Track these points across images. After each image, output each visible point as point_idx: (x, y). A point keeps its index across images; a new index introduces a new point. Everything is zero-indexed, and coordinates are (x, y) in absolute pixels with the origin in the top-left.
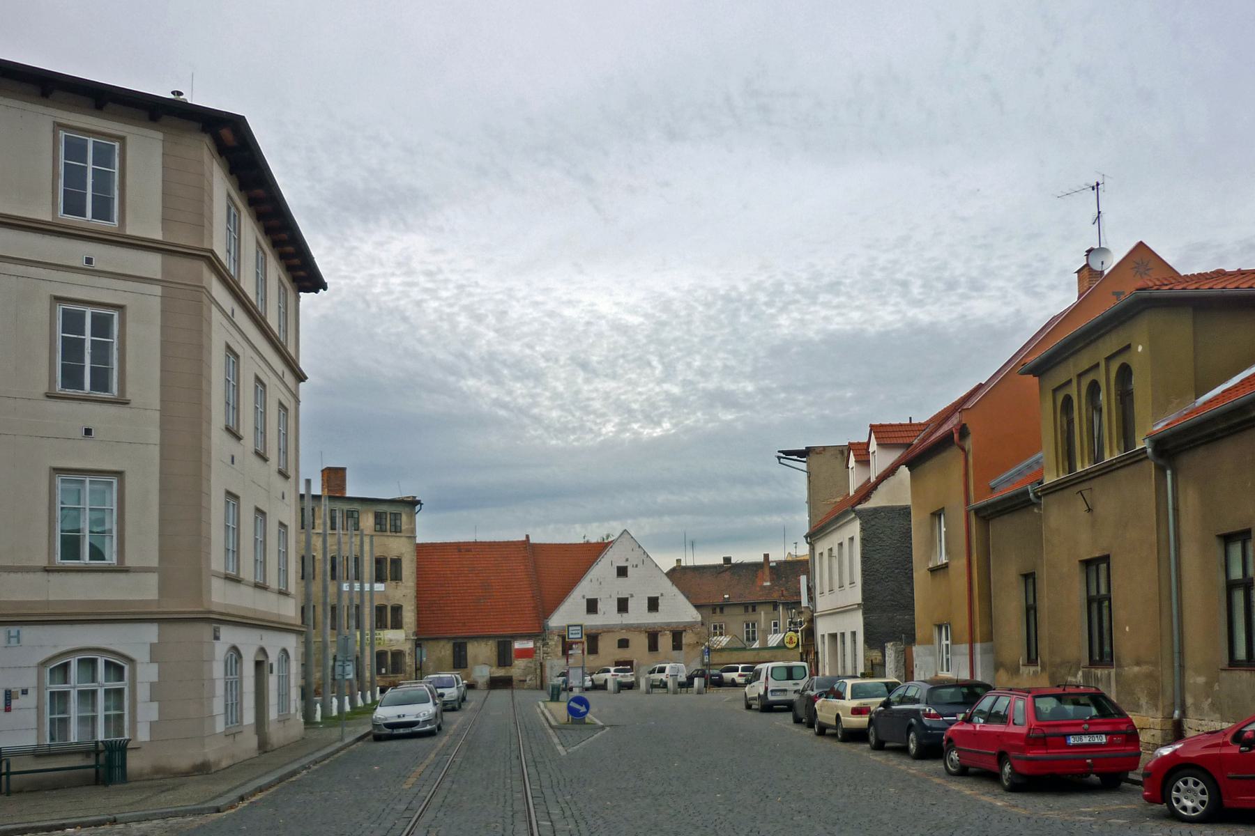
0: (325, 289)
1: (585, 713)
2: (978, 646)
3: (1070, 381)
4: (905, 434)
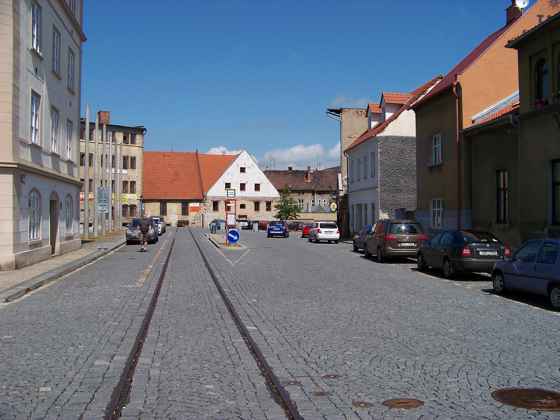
1: (236, 240)
2: (463, 212)
3: (546, 49)
4: (401, 99)
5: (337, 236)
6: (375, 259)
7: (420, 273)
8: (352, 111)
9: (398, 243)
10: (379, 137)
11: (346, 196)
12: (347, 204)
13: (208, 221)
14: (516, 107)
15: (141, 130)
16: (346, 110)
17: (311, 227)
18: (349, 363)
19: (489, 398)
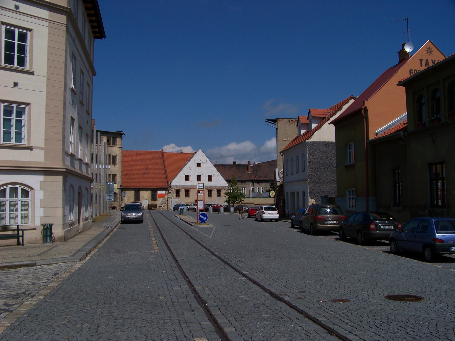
0: (105, 38)
1: (205, 220)
5: (277, 216)
6: (308, 233)
7: (341, 242)
8: (285, 120)
9: (325, 221)
10: (308, 143)
11: (282, 186)
12: (283, 191)
13: (172, 206)
14: (405, 125)
15: (120, 135)
16: (280, 120)
17: (257, 210)
18: (309, 287)
19: (383, 298)
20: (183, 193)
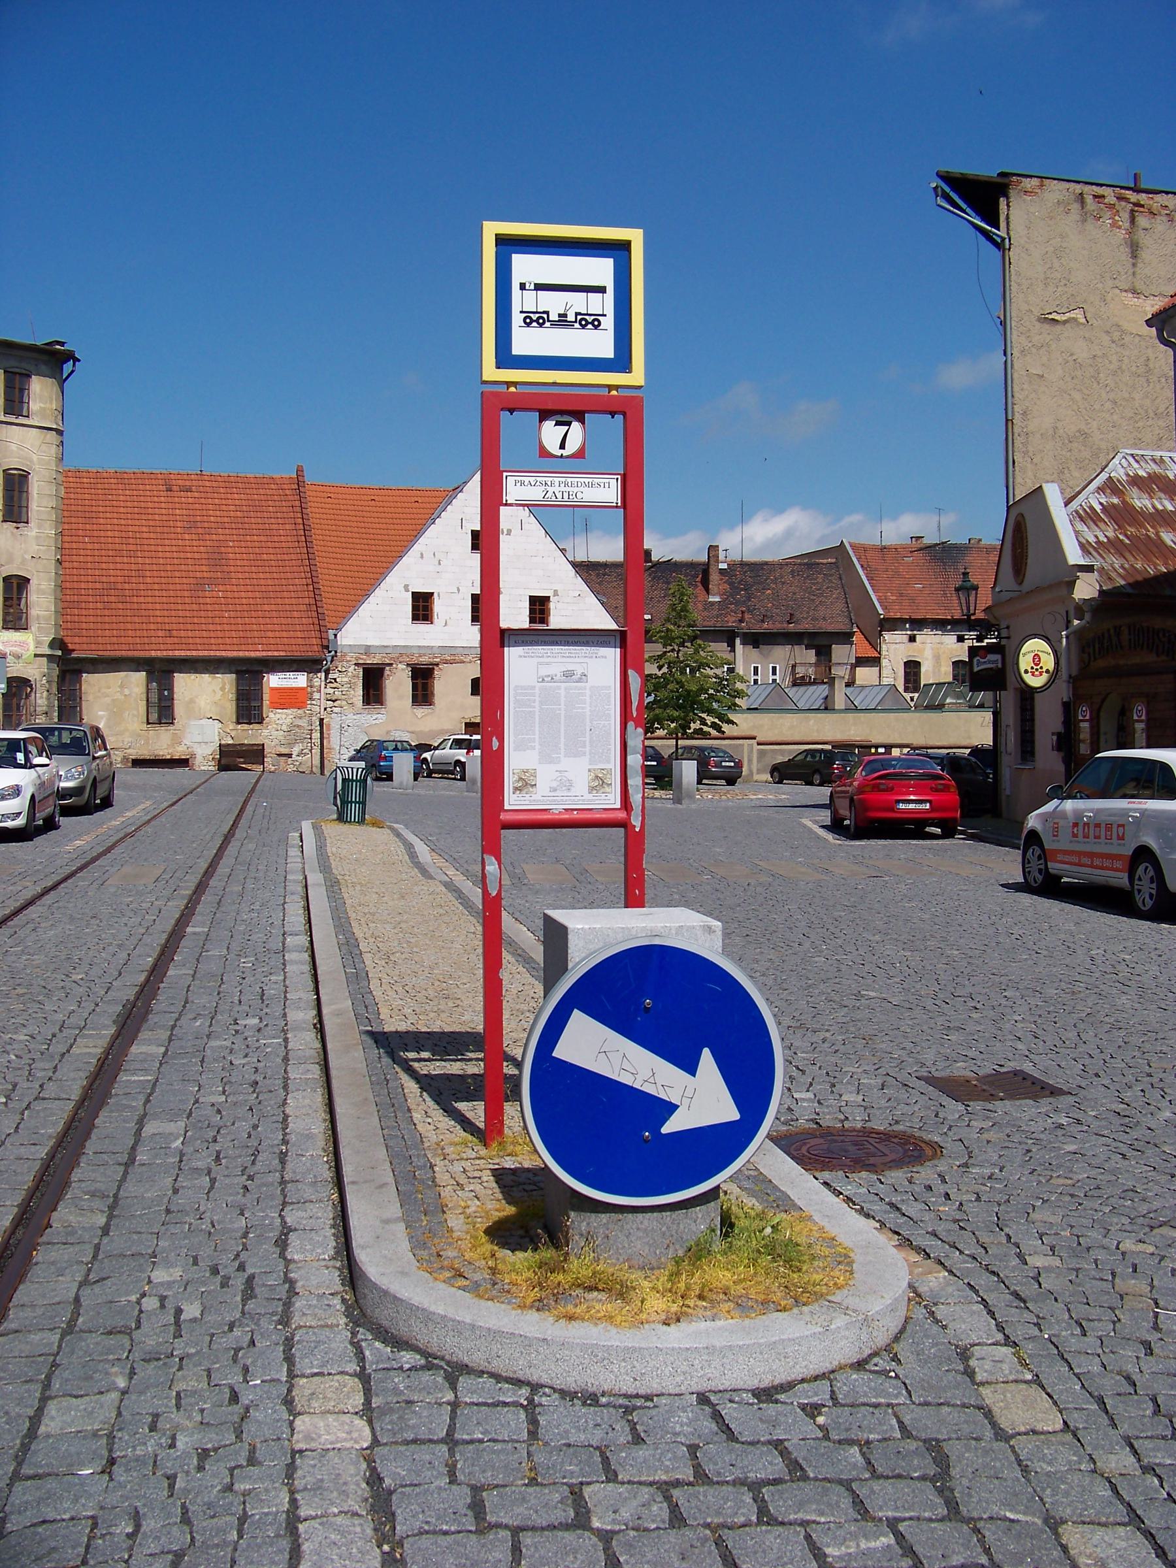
1: (717, 1146)
16: (1028, 184)
20: (398, 684)
